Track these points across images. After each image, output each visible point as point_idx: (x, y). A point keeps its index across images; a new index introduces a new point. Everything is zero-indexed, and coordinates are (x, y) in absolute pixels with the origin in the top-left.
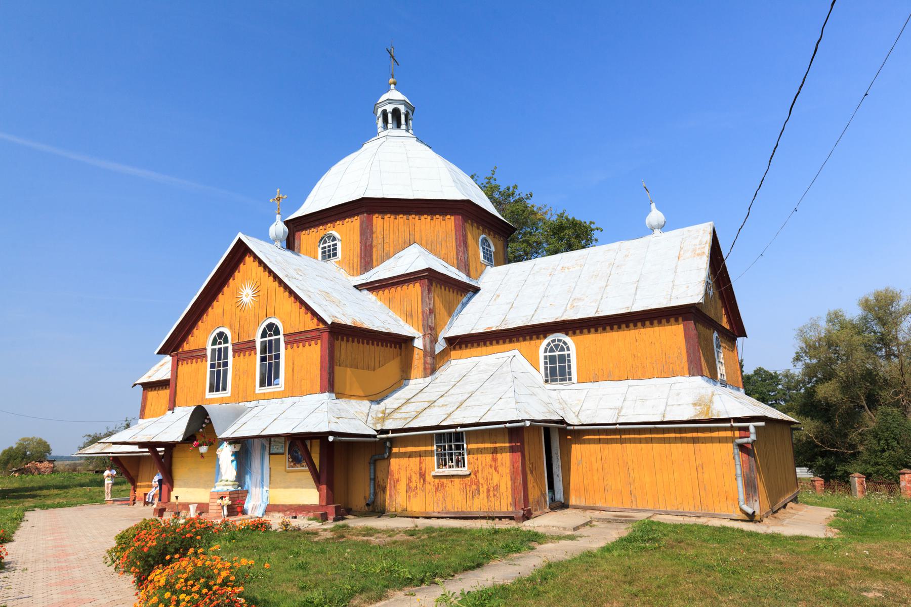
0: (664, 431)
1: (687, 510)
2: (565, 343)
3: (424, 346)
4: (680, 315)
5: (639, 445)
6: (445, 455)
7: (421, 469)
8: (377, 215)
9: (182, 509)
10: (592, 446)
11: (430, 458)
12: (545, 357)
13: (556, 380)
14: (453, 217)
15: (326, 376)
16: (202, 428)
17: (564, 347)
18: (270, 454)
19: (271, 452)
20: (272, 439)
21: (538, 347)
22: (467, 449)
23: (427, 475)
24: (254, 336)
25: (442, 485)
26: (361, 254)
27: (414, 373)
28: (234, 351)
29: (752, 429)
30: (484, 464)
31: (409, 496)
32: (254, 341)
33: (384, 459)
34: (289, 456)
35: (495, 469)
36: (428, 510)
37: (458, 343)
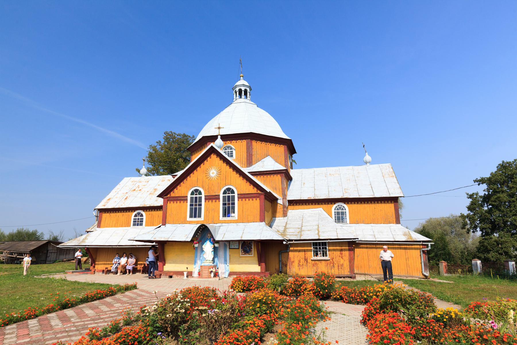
0: (396, 244)
1: (402, 275)
2: (344, 207)
3: (283, 203)
4: (393, 200)
5: (395, 250)
6: (317, 251)
7: (305, 257)
8: (254, 141)
9: (173, 274)
10: (364, 249)
11: (310, 252)
12: (335, 212)
13: (340, 222)
14: (283, 146)
15: (224, 211)
16: (197, 235)
17: (343, 209)
18: (230, 248)
19: (230, 248)
20: (231, 242)
21: (331, 208)
22: (328, 249)
23: (308, 260)
24: (220, 192)
25: (316, 264)
26: (247, 158)
27: (278, 214)
28: (206, 199)
29: (429, 245)
30: (336, 255)
31: (299, 269)
32: (219, 195)
33: (287, 252)
34: (242, 250)
35: (342, 257)
36: (309, 274)
37: (292, 203)
